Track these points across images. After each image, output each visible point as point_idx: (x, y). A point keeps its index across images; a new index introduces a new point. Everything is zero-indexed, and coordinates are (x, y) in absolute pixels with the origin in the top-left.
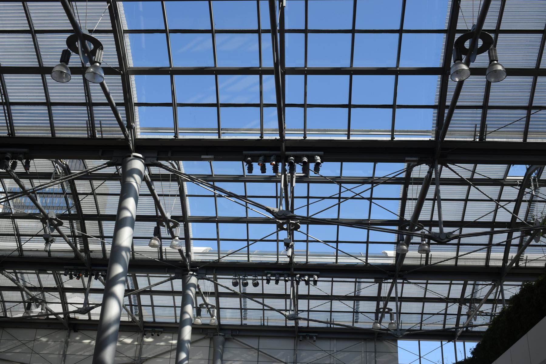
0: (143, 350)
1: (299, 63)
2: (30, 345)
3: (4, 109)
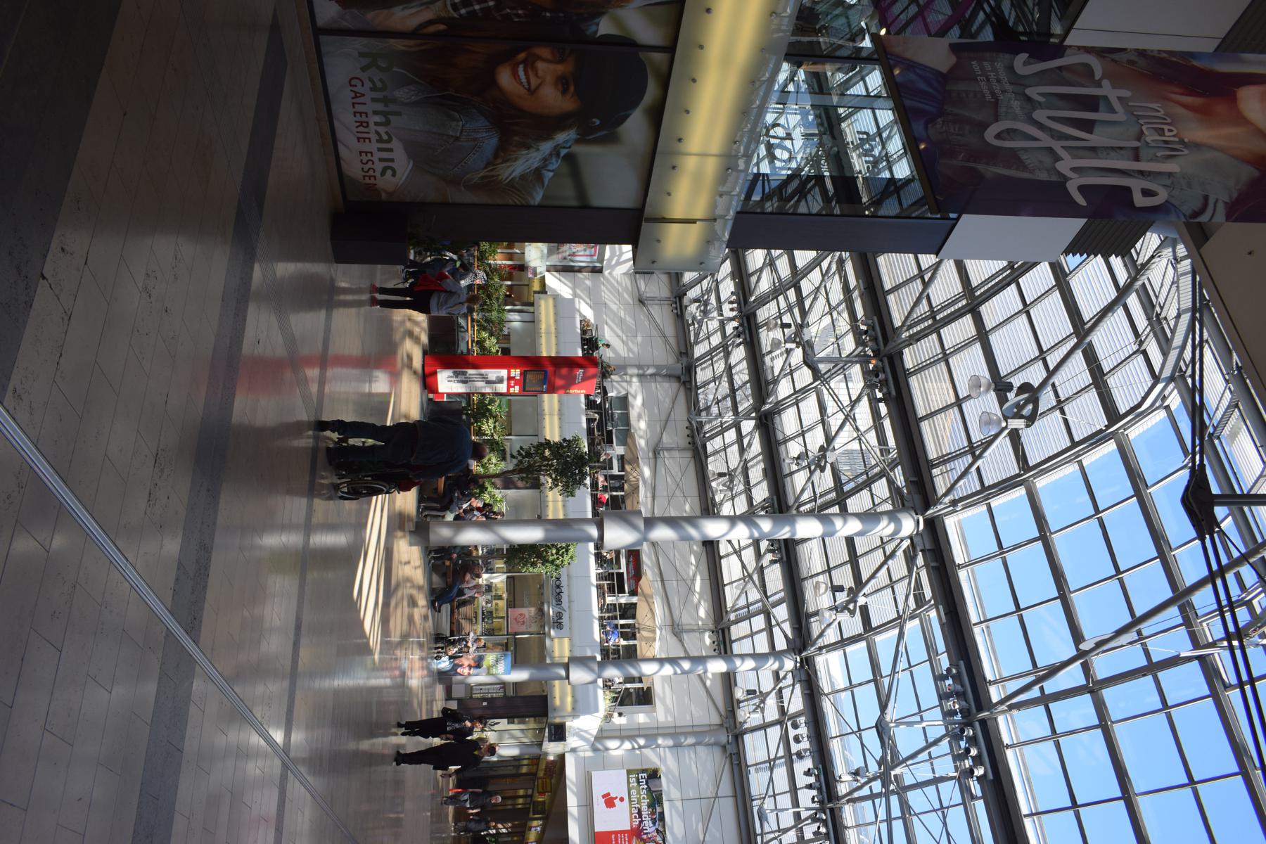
0: (692, 634)
1: (1115, 712)
2: (678, 493)
3: (937, 355)
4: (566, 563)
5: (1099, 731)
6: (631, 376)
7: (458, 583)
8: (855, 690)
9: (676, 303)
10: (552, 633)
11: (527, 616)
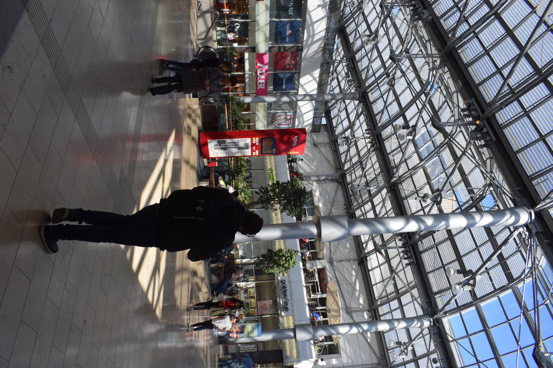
0: (358, 313)
4: (291, 265)
5: (494, 360)
6: (313, 181)
7: (227, 280)
8: (471, 337)
9: (333, 145)
10: (283, 314)
11: (268, 305)
